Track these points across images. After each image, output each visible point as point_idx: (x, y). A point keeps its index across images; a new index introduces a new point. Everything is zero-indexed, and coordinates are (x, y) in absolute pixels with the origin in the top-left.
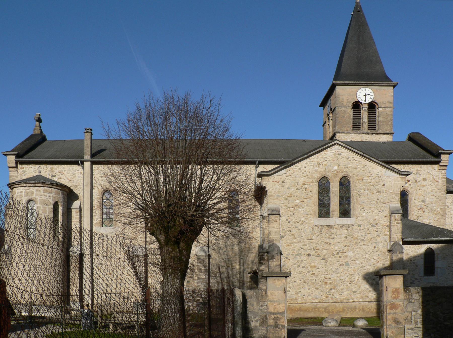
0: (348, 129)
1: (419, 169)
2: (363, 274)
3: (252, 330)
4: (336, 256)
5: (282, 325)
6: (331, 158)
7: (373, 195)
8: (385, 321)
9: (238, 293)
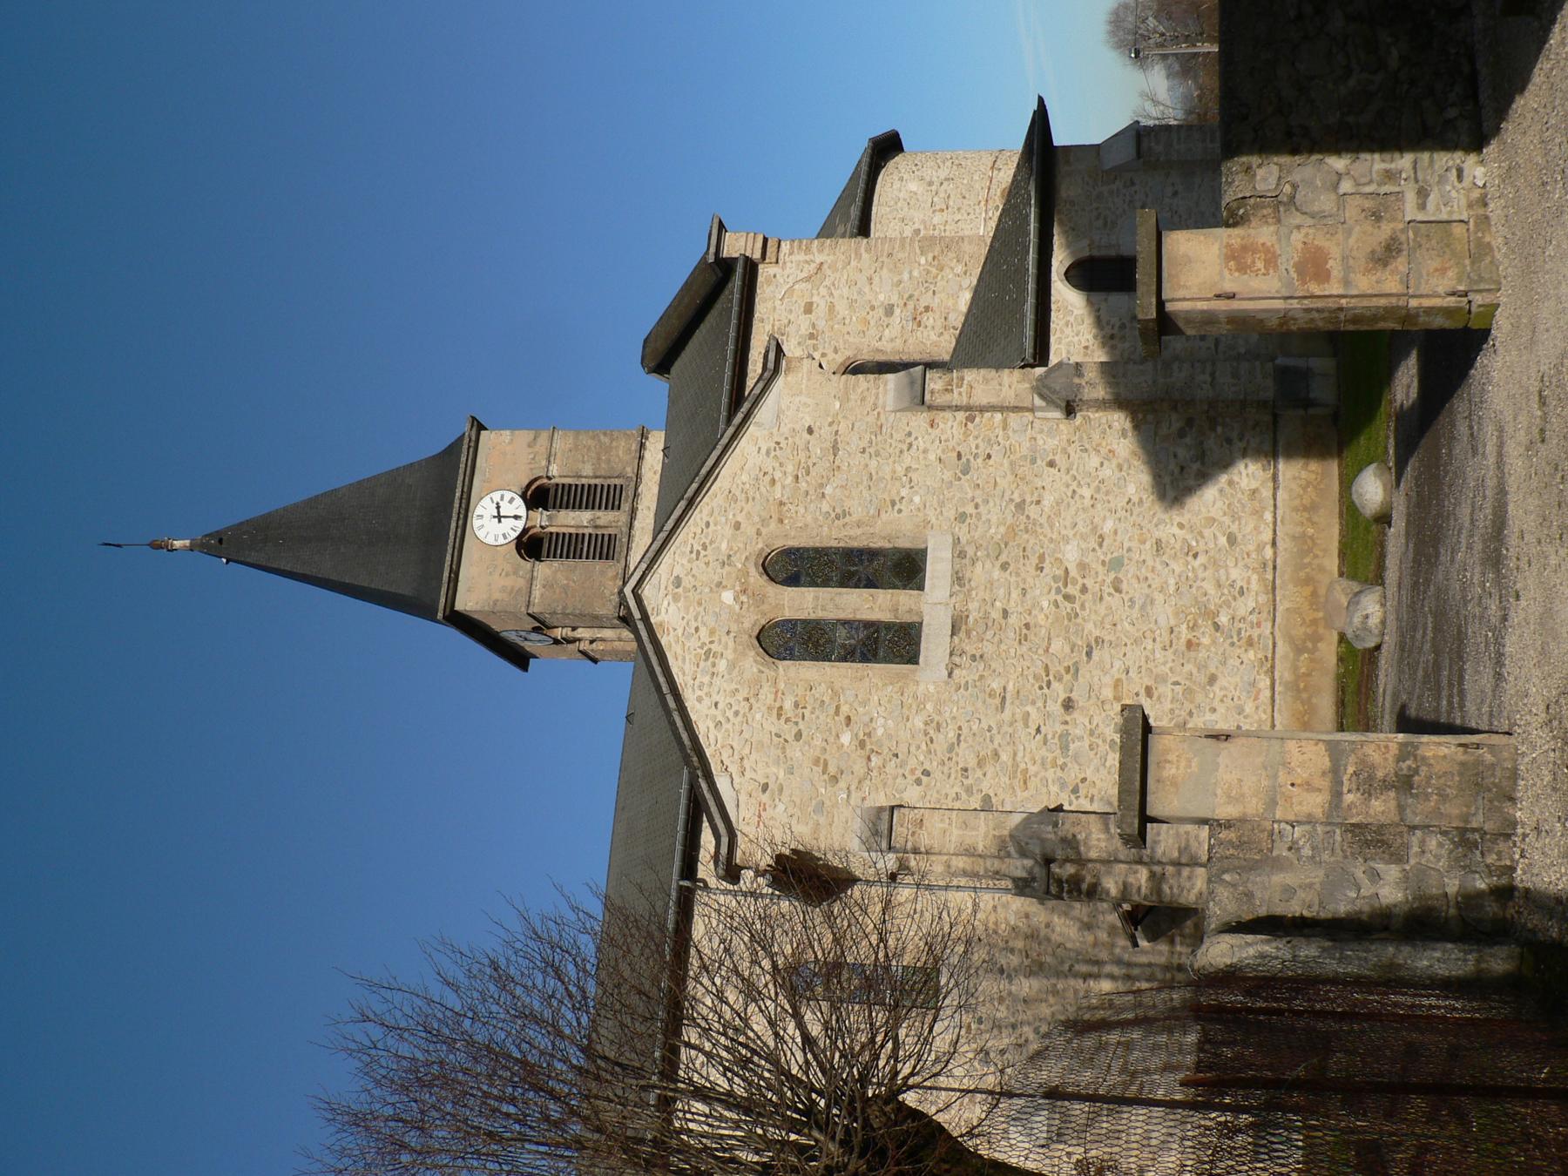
0: (611, 573)
2: (1158, 508)
3: (1421, 898)
4: (1077, 606)
5: (1401, 758)
6: (687, 609)
8: (1383, 302)
9: (1220, 952)
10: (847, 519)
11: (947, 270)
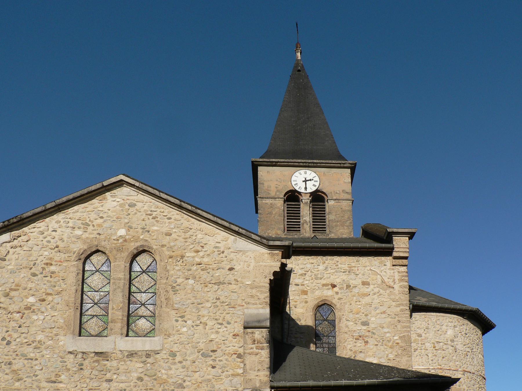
1: (353, 264)
6: (114, 211)
7: (206, 289)
10: (171, 293)
11: (390, 350)
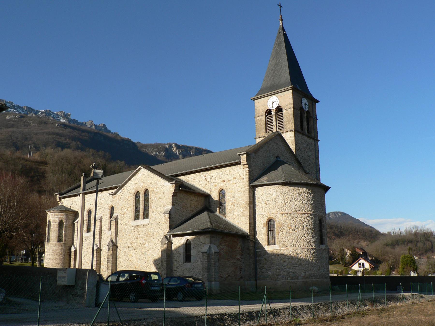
1: (230, 170)
